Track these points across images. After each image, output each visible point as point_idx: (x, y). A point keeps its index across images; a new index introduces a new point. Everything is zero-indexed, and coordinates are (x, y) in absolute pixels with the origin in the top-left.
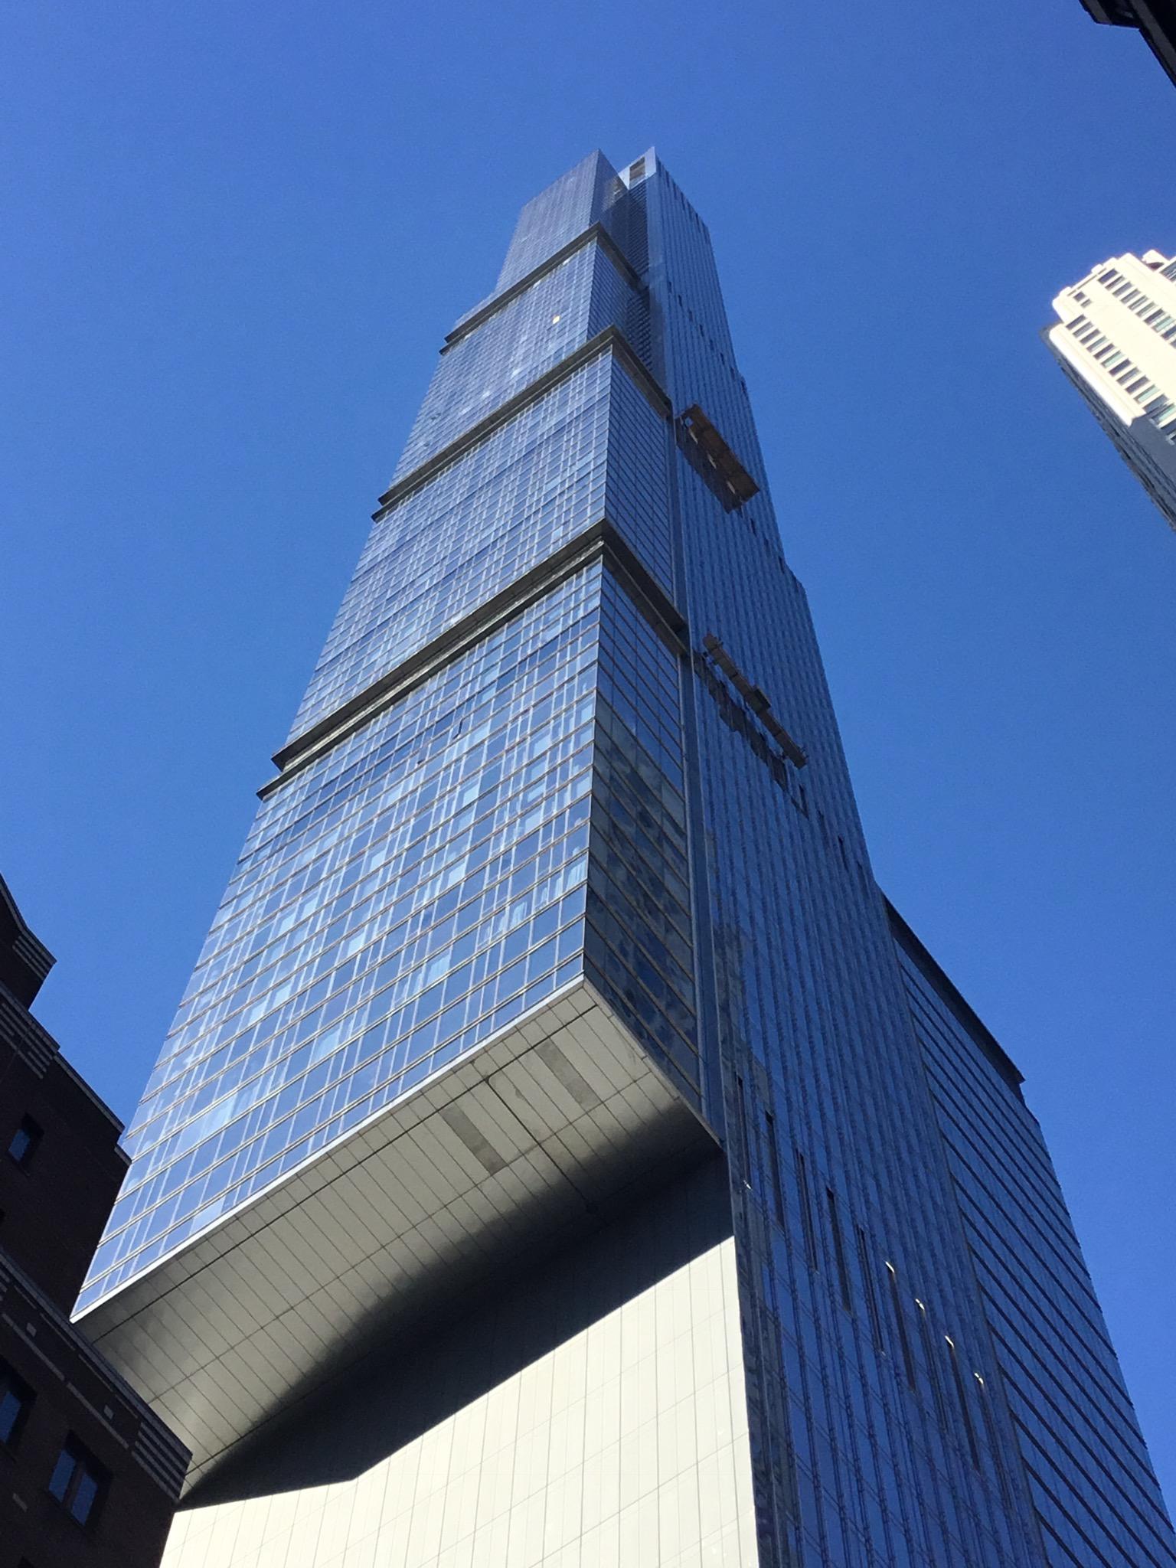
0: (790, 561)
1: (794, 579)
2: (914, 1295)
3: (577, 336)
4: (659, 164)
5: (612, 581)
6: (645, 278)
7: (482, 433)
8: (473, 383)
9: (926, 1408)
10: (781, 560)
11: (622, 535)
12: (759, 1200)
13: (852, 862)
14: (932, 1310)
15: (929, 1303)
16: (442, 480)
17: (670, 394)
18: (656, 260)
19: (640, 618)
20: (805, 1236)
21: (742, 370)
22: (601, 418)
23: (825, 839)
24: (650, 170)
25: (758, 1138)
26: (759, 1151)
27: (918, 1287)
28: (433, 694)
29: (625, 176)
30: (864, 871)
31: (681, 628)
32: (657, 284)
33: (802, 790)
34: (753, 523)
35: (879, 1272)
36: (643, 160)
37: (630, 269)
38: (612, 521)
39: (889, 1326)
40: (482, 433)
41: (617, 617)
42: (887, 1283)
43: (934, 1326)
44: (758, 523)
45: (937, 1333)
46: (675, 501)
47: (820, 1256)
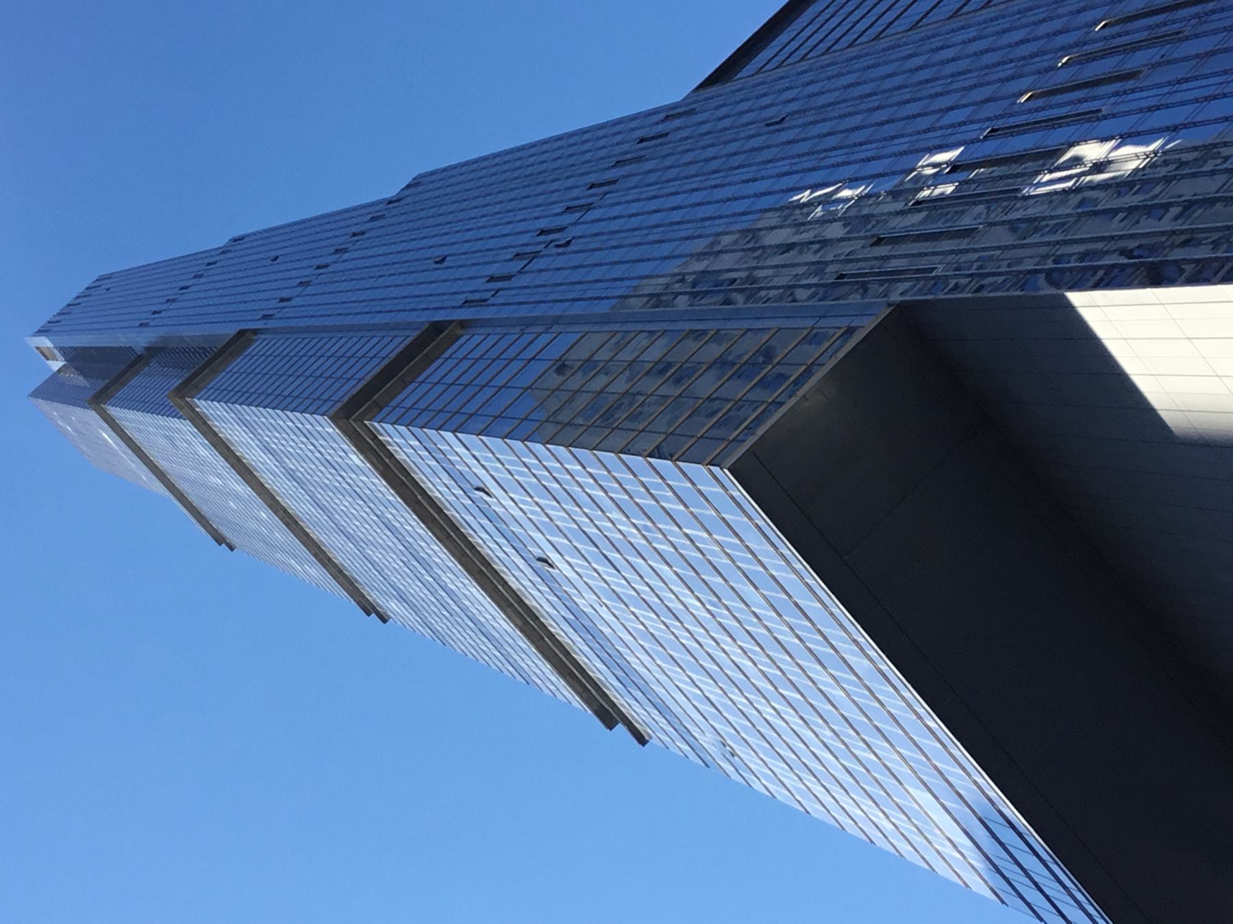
0: (391, 192)
1: (408, 186)
2: (1053, 68)
3: (184, 428)
4: (42, 332)
5: (386, 410)
6: (139, 351)
7: (291, 522)
8: (252, 525)
9: (1157, 59)
10: (390, 202)
11: (349, 395)
12: (1193, 22)
13: (660, 128)
14: (1071, 47)
15: (1065, 49)
16: (339, 559)
17: (231, 330)
18: (120, 339)
19: (446, 355)
20: (1148, 47)
21: (221, 241)
22: (252, 413)
23: (639, 159)
24: (46, 342)
25: (1072, 103)
26: (1059, 106)
27: (1046, 64)
28: (520, 578)
29: (56, 365)
30: (671, 113)
31: (437, 328)
32: (140, 340)
33: (592, 186)
34: (354, 235)
35: (1030, 111)
36: (38, 348)
37: (134, 363)
38: (335, 409)
39: (1080, 101)
40: (291, 522)
41: (470, 362)
42: (1116, 29)
43: (1085, 44)
44: (354, 229)
45: (1095, 41)
46: (325, 329)
47: (1084, 107)
